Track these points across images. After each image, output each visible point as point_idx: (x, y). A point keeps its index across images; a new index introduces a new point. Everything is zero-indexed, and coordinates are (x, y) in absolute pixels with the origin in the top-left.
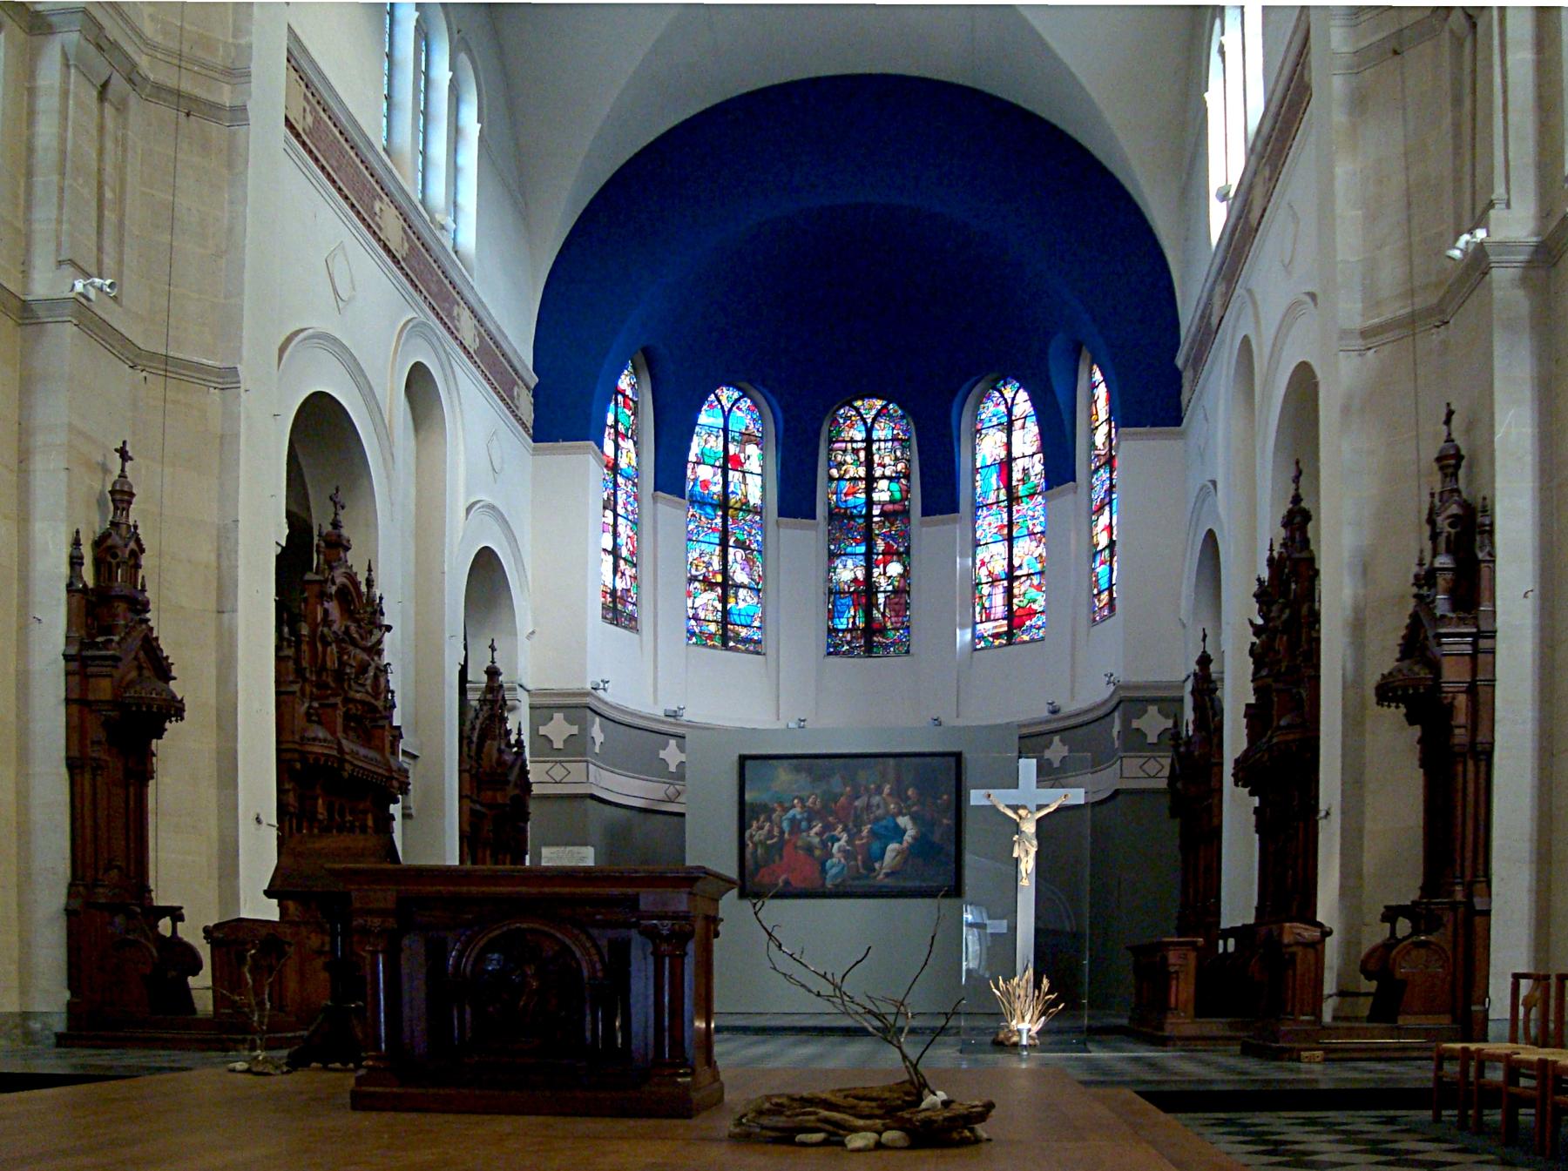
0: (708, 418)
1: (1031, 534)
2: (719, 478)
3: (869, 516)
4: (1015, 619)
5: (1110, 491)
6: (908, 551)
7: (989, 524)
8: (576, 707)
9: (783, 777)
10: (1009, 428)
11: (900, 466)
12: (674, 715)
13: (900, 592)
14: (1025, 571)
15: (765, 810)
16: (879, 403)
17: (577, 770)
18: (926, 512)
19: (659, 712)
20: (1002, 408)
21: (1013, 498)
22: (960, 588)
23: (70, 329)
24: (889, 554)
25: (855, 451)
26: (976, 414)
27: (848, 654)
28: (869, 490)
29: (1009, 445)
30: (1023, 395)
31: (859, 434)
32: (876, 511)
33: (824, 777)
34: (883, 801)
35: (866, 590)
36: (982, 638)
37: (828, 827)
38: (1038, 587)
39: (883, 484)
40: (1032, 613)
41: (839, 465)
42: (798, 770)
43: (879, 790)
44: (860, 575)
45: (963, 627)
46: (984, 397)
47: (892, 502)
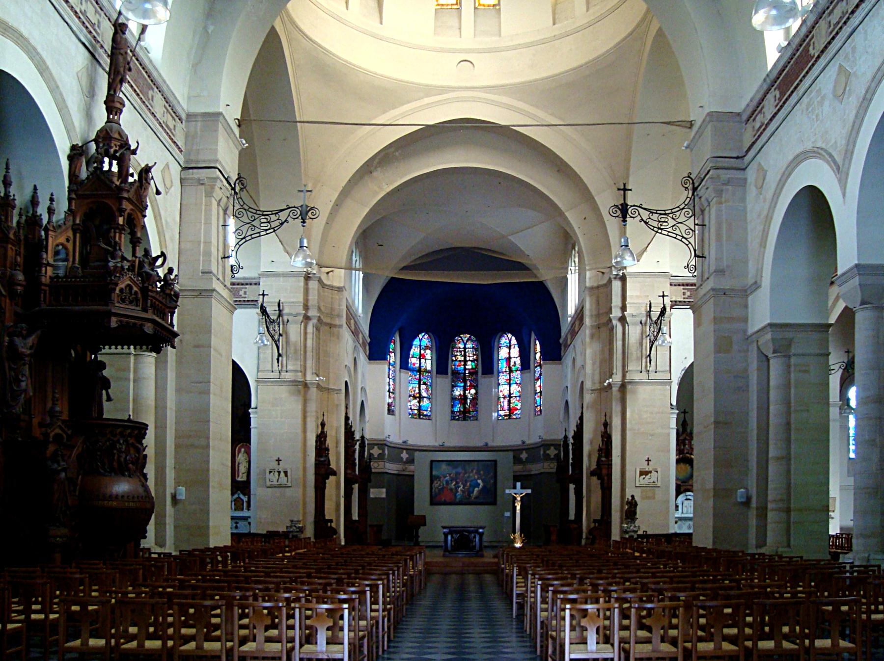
0: (416, 342)
1: (516, 383)
2: (418, 362)
3: (465, 373)
4: (511, 410)
5: (541, 375)
6: (477, 385)
7: (503, 378)
8: (381, 444)
9: (444, 466)
10: (510, 348)
11: (475, 357)
12: (405, 442)
13: (475, 399)
14: (514, 395)
15: (438, 478)
16: (468, 336)
17: (381, 464)
18: (483, 373)
19: (401, 442)
20: (508, 341)
21: (511, 371)
22: (494, 399)
23: (315, 389)
24: (471, 387)
25: (461, 352)
26: (499, 341)
27: (458, 420)
28: (465, 365)
29: (509, 353)
30: (513, 338)
31: (462, 346)
32: (467, 372)
33: (456, 467)
34: (473, 475)
35: (463, 398)
36: (501, 416)
37: (457, 483)
38: (519, 401)
39: (469, 363)
40: (516, 409)
41: (455, 356)
42: (448, 465)
43: (472, 471)
44: (462, 393)
45: (495, 412)
46: (502, 336)
47: (472, 369)
